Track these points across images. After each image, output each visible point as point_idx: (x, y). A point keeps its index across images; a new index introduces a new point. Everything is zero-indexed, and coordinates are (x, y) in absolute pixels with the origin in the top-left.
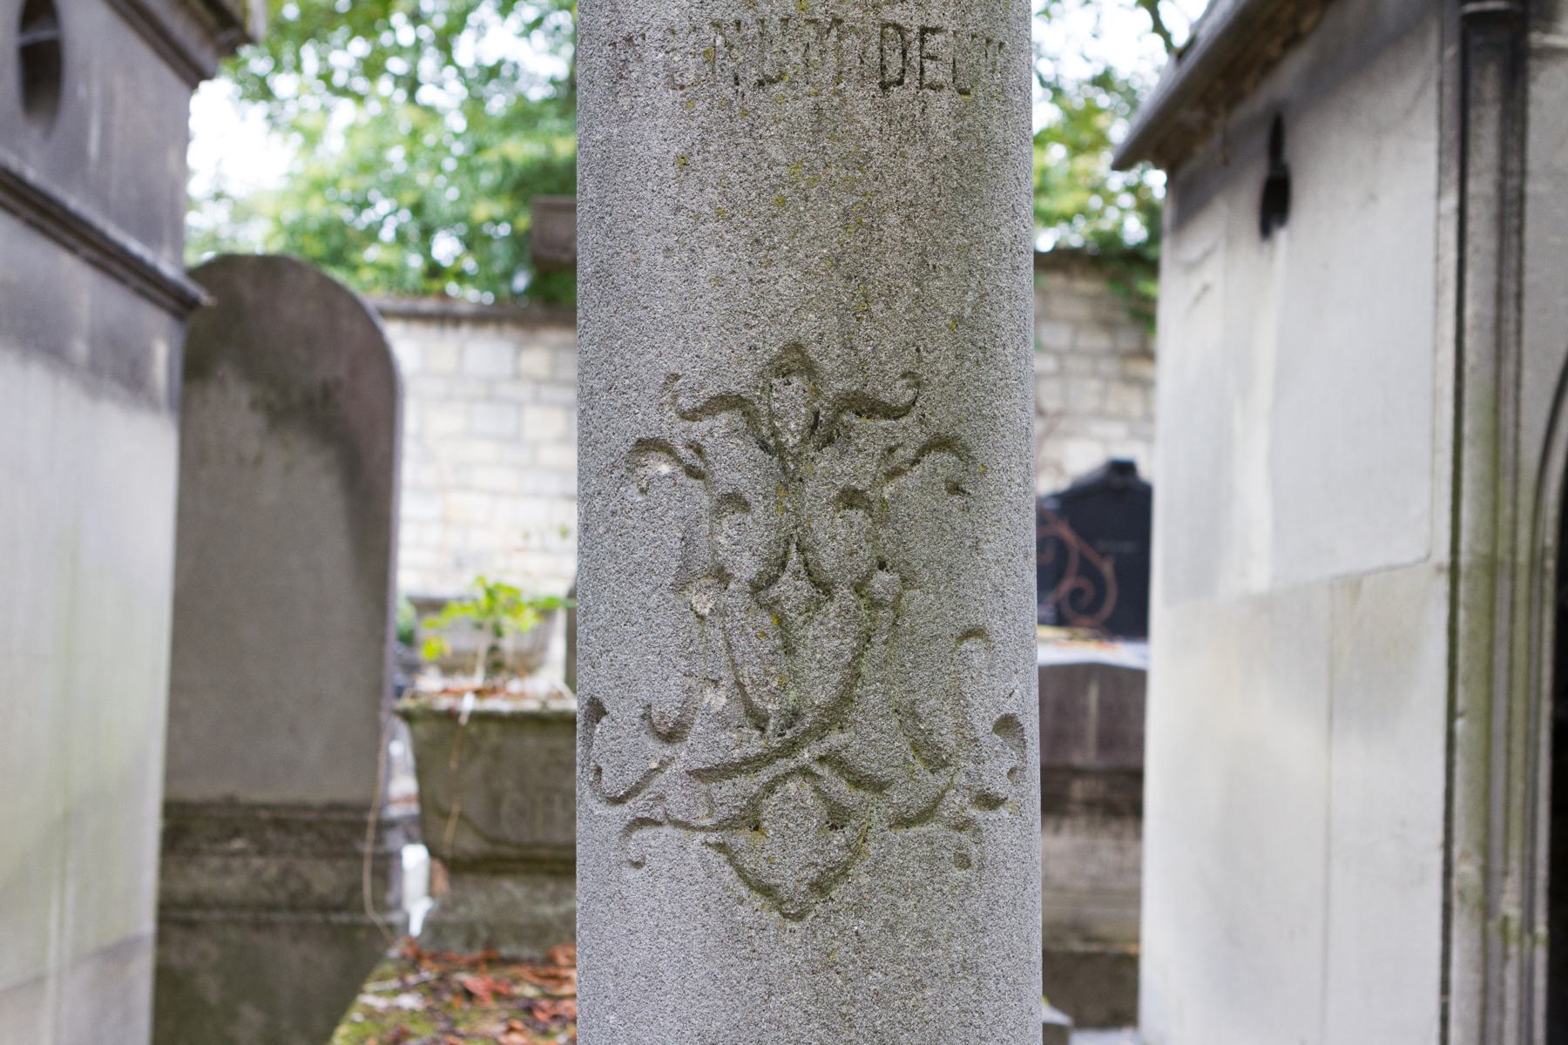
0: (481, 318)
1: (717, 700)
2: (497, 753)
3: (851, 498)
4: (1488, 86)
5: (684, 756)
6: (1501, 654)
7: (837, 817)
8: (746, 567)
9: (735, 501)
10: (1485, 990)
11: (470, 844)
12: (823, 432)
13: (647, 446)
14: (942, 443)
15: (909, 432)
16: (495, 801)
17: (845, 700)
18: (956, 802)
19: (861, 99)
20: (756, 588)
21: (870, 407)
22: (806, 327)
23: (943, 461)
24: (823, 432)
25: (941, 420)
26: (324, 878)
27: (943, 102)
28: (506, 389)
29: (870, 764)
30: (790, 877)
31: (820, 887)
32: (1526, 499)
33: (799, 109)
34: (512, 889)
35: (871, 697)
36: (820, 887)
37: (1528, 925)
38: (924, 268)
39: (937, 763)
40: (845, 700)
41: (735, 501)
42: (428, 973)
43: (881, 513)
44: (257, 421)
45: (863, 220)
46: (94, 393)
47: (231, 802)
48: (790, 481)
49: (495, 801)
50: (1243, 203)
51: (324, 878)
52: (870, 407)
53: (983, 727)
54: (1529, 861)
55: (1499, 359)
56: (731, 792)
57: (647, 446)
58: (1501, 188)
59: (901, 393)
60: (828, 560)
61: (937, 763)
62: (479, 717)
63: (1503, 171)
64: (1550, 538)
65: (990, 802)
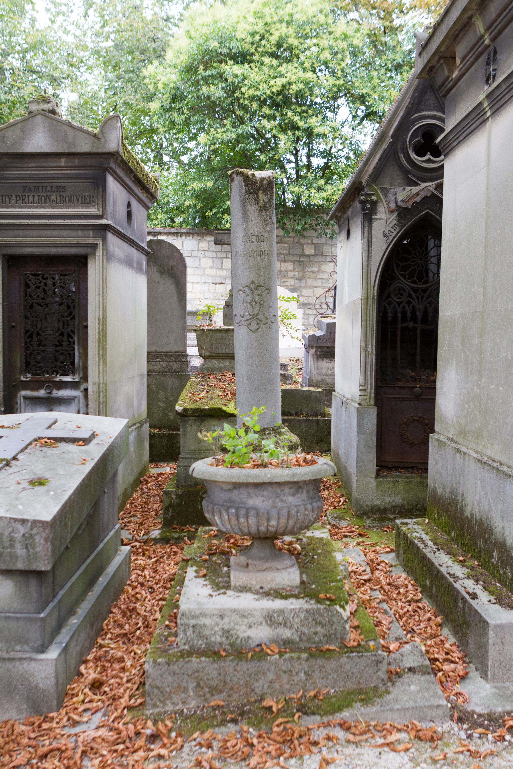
0: (188, 234)
1: (247, 313)
2: (212, 337)
3: (258, 295)
4: (366, 225)
5: (244, 319)
6: (368, 312)
7: (258, 324)
8: (249, 301)
9: (248, 295)
10: (366, 362)
11: (207, 354)
12: (256, 289)
13: (240, 290)
14: (267, 289)
15: (264, 288)
16: (212, 345)
17: (258, 313)
18: (269, 322)
19: (259, 258)
20: (250, 303)
21: (260, 286)
22: (254, 279)
23: (267, 291)
24: (256, 289)
25: (267, 287)
26: (175, 366)
27: (266, 257)
28: (195, 253)
29: (261, 319)
30: (254, 329)
31: (257, 330)
32: (372, 288)
33: (253, 259)
34: (215, 362)
35: (261, 313)
36: (257, 330)
37: (372, 352)
38: (265, 273)
39: (267, 319)
40: (258, 313)
41: (248, 295)
42: (201, 375)
43: (261, 296)
44: (158, 274)
45: (259, 269)
46: (137, 273)
47: (156, 351)
48: (253, 293)
49: (212, 345)
50: (344, 234)
51: (175, 366)
52: (260, 286)
53: (272, 315)
54: (372, 343)
55: (368, 267)
56: (248, 322)
57: (240, 290)
58: (368, 240)
59: (263, 285)
60: (257, 300)
61: (267, 319)
62: (208, 330)
63: (369, 237)
64: (375, 294)
65: (273, 323)
